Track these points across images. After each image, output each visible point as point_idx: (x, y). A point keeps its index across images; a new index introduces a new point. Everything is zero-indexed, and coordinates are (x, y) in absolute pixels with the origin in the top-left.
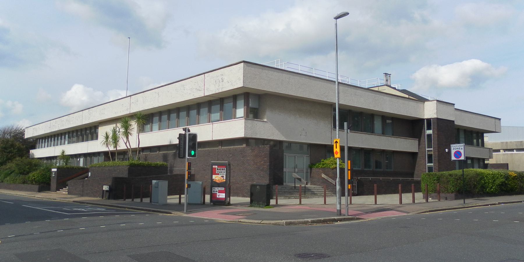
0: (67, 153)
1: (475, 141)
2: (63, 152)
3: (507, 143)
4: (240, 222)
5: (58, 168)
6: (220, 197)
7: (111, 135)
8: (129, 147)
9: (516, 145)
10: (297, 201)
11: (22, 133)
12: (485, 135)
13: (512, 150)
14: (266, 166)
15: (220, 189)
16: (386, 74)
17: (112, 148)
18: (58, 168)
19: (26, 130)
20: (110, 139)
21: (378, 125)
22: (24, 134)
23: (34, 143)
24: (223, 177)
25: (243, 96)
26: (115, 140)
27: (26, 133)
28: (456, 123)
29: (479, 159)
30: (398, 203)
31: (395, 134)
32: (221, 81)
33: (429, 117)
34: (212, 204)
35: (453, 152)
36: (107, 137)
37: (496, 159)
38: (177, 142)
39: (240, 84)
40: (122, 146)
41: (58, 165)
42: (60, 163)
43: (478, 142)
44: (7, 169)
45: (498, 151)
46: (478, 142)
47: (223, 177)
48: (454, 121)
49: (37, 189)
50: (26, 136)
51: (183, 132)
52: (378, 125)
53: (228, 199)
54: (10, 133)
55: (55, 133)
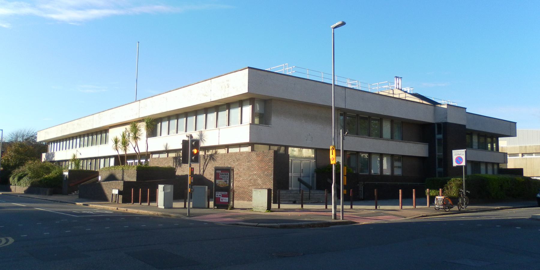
0: (79, 157)
1: (489, 146)
2: (74, 156)
3: (526, 147)
4: (238, 224)
5: (70, 172)
6: (224, 201)
7: (120, 138)
8: (138, 152)
9: (536, 149)
10: (374, 207)
11: (34, 137)
12: (499, 139)
13: (531, 154)
14: (271, 171)
15: (223, 193)
16: (396, 77)
17: (121, 152)
18: (70, 172)
19: (38, 133)
20: (120, 144)
21: (387, 128)
22: (36, 138)
23: (43, 147)
24: (226, 181)
25: (225, 106)
26: (125, 144)
27: (38, 136)
28: (467, 127)
29: (493, 164)
30: (277, 207)
31: (403, 139)
32: (227, 86)
33: (439, 122)
34: (216, 207)
35: (454, 157)
36: (116, 142)
37: (512, 164)
38: (180, 147)
39: (245, 90)
40: (131, 150)
41: (70, 168)
42: (72, 166)
43: (492, 146)
44: (20, 172)
45: (516, 155)
46: (492, 146)
47: (226, 181)
48: (464, 126)
49: (48, 192)
50: (38, 140)
51: (187, 139)
52: (387, 128)
53: (232, 202)
54: (23, 136)
55: (70, 136)
